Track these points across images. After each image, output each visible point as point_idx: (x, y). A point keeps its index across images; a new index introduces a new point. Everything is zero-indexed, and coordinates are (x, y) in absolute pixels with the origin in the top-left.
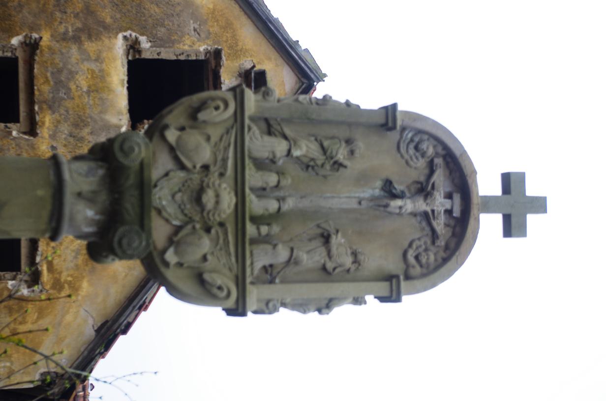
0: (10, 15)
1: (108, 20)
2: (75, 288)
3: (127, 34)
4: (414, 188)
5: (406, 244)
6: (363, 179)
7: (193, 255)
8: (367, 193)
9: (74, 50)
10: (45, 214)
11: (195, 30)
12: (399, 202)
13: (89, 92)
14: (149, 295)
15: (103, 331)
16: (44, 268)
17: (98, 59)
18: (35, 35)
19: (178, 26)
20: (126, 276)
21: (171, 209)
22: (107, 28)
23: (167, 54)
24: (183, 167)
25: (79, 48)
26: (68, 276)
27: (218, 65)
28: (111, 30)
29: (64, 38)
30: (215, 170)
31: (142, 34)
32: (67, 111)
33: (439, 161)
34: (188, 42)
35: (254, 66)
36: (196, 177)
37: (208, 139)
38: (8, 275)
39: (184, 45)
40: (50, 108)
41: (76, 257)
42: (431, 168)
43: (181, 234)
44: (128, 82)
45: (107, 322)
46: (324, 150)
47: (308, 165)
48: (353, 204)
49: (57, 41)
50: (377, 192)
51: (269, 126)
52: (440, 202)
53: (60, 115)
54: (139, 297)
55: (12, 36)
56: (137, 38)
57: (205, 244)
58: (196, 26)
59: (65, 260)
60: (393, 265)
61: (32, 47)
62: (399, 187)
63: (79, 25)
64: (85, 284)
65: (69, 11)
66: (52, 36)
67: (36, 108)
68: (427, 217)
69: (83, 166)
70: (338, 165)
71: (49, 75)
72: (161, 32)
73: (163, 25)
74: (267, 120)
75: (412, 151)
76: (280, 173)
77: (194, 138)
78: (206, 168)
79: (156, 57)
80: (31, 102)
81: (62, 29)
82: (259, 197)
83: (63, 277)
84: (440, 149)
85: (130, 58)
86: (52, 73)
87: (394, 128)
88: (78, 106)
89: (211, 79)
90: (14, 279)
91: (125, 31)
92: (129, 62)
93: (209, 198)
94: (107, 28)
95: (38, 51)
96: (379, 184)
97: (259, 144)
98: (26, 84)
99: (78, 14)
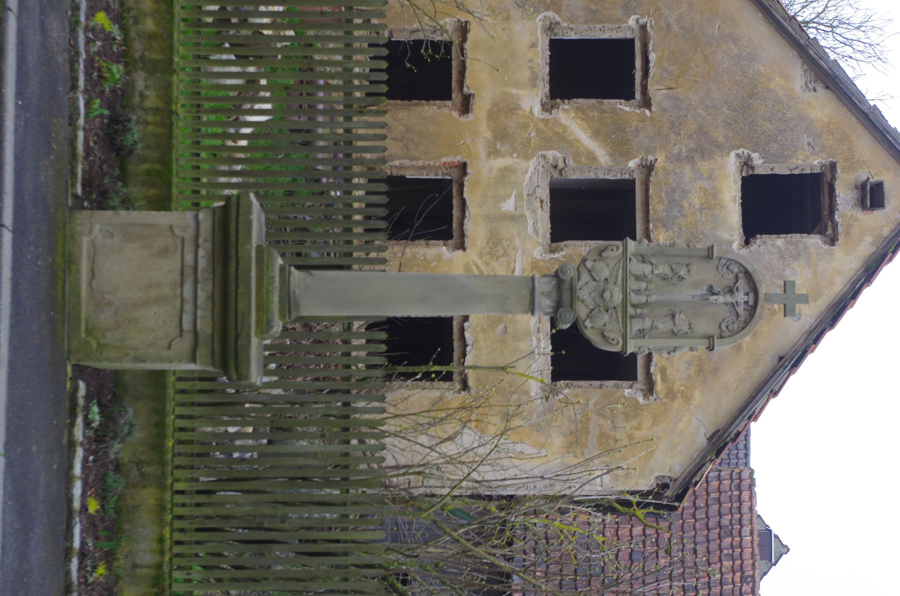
0: (627, 140)
1: (721, 139)
2: (687, 398)
3: (740, 151)
4: (726, 290)
5: (721, 319)
6: (696, 285)
7: (599, 323)
8: (698, 292)
9: (687, 169)
10: (527, 302)
11: (809, 144)
12: (715, 297)
13: (701, 210)
14: (759, 406)
15: (714, 439)
16: (658, 378)
17: (710, 177)
18: (651, 158)
19: (792, 141)
20: (737, 387)
21: (589, 301)
22: (719, 147)
23: (782, 170)
24: (595, 280)
25: (692, 168)
26: (681, 385)
27: (833, 178)
28: (723, 149)
29: (678, 158)
30: (611, 281)
31: (755, 151)
32: (680, 229)
33: (741, 275)
34: (801, 157)
35: (868, 178)
36: (602, 285)
37: (608, 265)
38: (626, 383)
39: (797, 160)
40: (664, 225)
41: (688, 368)
42: (737, 279)
43: (594, 312)
44: (742, 198)
45: (718, 431)
46: (672, 270)
47: (664, 278)
48: (690, 299)
49: (672, 162)
50: (704, 292)
51: (643, 258)
52: (741, 297)
53: (674, 233)
54: (749, 408)
55: (630, 160)
56: (749, 156)
57: (606, 318)
58: (810, 140)
59: (677, 371)
60: (713, 330)
61: (648, 168)
62: (716, 289)
63: (692, 145)
64: (697, 394)
65: (683, 133)
66: (666, 157)
67: (651, 226)
68: (733, 305)
69: (546, 280)
70: (681, 278)
71: (663, 194)
72: (774, 148)
73: (776, 141)
74: (642, 255)
75: (725, 270)
76: (649, 282)
77: (601, 265)
78: (606, 280)
79: (770, 172)
80: (647, 221)
81: (676, 150)
82: (636, 294)
83: (676, 387)
84: (741, 269)
85: (744, 175)
86: (666, 192)
87: (712, 258)
88: (691, 223)
89: (826, 191)
90: (631, 387)
91: (738, 149)
92: (743, 179)
93: (607, 295)
94: (719, 147)
95: (653, 173)
96: (706, 287)
97: (636, 267)
98: (642, 204)
99: (691, 135)
